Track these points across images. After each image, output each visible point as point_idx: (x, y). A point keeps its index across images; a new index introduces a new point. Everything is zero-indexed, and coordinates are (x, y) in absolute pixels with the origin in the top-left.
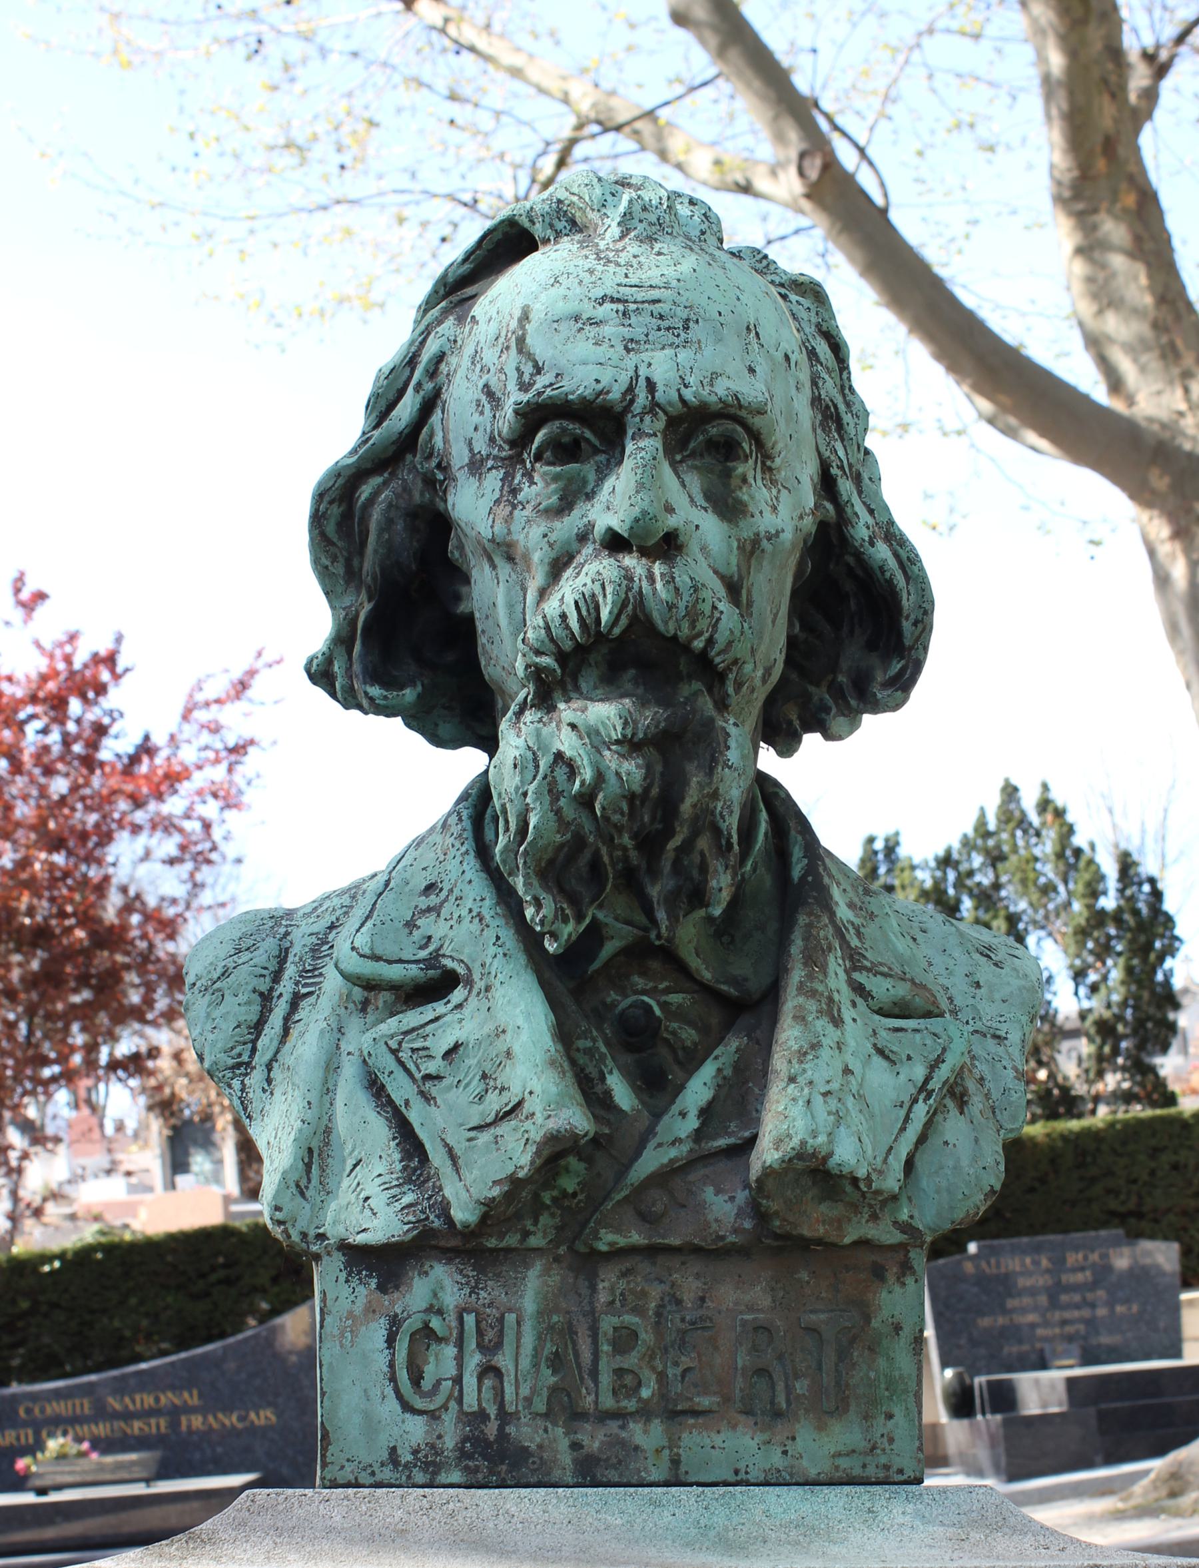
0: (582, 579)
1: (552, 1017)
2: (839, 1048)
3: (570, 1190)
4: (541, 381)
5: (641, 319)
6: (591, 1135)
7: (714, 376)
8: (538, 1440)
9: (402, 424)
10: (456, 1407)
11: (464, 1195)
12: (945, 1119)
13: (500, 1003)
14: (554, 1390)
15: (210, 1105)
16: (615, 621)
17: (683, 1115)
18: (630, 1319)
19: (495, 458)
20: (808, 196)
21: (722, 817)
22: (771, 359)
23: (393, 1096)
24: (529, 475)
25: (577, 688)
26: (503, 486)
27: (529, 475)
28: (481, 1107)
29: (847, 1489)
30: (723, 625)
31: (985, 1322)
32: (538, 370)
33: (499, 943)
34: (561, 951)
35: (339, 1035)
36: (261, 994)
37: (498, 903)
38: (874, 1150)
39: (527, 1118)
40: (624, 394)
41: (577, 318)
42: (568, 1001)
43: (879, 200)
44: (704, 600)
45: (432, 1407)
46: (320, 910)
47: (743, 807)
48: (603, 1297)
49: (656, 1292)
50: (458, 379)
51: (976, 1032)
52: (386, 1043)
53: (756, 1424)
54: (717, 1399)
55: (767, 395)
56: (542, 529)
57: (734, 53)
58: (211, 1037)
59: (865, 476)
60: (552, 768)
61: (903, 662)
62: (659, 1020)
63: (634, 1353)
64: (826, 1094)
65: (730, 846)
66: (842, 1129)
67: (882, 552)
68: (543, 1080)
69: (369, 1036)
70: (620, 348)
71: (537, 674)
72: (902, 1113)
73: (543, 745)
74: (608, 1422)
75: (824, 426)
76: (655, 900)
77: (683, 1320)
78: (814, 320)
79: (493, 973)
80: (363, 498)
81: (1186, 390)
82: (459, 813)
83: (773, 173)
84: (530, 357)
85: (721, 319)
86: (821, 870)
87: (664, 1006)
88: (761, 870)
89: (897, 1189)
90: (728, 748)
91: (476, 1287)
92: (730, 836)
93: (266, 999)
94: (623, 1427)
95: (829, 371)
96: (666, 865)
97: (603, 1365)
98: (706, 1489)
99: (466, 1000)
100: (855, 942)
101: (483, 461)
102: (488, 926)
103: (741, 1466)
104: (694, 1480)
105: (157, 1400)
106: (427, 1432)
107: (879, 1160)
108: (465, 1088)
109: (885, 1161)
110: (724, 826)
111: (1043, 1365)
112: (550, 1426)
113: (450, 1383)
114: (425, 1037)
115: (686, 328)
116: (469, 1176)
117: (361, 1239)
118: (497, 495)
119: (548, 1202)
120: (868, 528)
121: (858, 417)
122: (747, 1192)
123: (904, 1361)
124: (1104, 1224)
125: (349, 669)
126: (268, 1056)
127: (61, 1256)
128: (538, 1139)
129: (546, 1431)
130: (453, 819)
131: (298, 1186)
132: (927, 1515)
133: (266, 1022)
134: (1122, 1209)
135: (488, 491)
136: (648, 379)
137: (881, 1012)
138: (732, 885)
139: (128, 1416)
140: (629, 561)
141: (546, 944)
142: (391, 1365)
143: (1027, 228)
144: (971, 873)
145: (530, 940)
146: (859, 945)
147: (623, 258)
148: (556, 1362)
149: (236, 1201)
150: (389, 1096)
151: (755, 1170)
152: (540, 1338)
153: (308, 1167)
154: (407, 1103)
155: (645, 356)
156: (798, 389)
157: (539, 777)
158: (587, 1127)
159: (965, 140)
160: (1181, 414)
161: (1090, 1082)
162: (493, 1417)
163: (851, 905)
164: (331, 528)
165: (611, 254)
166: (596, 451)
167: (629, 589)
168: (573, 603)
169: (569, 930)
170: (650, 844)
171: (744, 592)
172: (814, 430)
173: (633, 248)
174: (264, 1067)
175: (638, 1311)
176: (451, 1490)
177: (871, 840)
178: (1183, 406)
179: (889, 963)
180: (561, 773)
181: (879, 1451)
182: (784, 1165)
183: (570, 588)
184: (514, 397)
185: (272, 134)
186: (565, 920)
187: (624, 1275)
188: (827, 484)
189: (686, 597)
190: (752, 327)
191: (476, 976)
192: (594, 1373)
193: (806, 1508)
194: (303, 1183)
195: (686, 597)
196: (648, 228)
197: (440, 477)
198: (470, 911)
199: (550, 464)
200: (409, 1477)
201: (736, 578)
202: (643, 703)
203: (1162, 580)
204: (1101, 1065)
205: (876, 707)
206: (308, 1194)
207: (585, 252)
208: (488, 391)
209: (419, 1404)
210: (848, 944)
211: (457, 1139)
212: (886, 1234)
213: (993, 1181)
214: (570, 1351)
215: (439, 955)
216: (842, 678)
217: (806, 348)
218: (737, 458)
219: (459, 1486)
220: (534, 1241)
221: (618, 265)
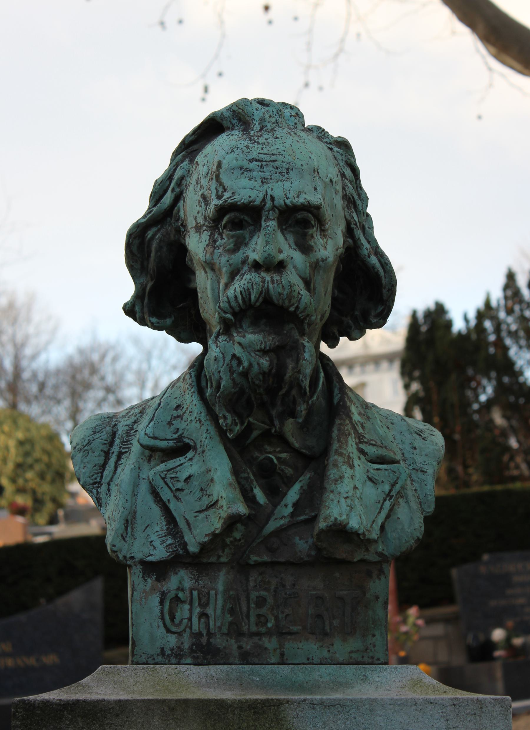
0: (243, 282)
1: (230, 464)
2: (352, 478)
3: (238, 538)
5: (268, 169)
6: (247, 515)
7: (299, 193)
8: (224, 645)
9: (166, 206)
10: (189, 631)
11: (193, 540)
12: (398, 508)
13: (208, 458)
14: (231, 624)
17: (286, 506)
18: (263, 593)
19: (207, 226)
21: (302, 381)
22: (325, 183)
23: (163, 498)
24: (221, 234)
25: (241, 327)
26: (210, 239)
27: (221, 234)
28: (200, 503)
29: (355, 666)
30: (302, 301)
31: (493, 603)
32: (225, 190)
33: (208, 432)
34: (234, 437)
35: (139, 471)
36: (105, 452)
37: (207, 415)
38: (366, 521)
39: (220, 508)
40: (261, 202)
41: (241, 168)
44: (294, 291)
45: (179, 631)
46: (129, 414)
47: (311, 378)
48: (252, 584)
50: (190, 188)
51: (414, 469)
52: (160, 475)
53: (317, 638)
54: (300, 628)
55: (322, 199)
56: (227, 258)
58: (83, 471)
59: (366, 226)
60: (231, 361)
61: (383, 307)
62: (276, 465)
63: (265, 608)
64: (346, 498)
65: (305, 393)
66: (353, 513)
67: (374, 260)
68: (226, 492)
69: (152, 472)
70: (259, 182)
72: (379, 506)
74: (254, 637)
75: (348, 207)
76: (274, 416)
77: (286, 594)
78: (344, 159)
79: (206, 445)
80: (149, 236)
82: (190, 374)
84: (221, 184)
85: (303, 168)
86: (346, 399)
87: (278, 459)
88: (321, 399)
89: (376, 538)
90: (305, 352)
91: (198, 579)
92: (305, 389)
93: (107, 454)
94: (260, 640)
95: (351, 182)
97: (252, 613)
98: (296, 666)
99: (194, 456)
100: (361, 430)
101: (201, 227)
102: (203, 425)
103: (310, 656)
104: (290, 662)
106: (177, 641)
107: (369, 526)
108: (193, 494)
109: (371, 526)
110: (303, 385)
112: (229, 639)
113: (187, 620)
114: (177, 472)
115: (288, 172)
116: (196, 532)
117: (150, 559)
118: (207, 242)
119: (229, 543)
120: (367, 250)
121: (363, 200)
122: (313, 539)
123: (380, 612)
125: (142, 309)
126: (108, 479)
128: (224, 517)
129: (227, 641)
130: (187, 377)
131: (122, 536)
132: (388, 677)
133: (107, 464)
135: (204, 240)
136: (271, 196)
137: (372, 462)
138: (306, 409)
141: (228, 434)
142: (162, 613)
145: (222, 433)
146: (363, 432)
147: (262, 140)
148: (232, 612)
150: (160, 497)
151: (316, 531)
152: (225, 601)
153: (126, 528)
154: (169, 500)
155: (270, 185)
156: (336, 194)
157: (225, 365)
158: (245, 512)
162: (205, 635)
163: (360, 414)
164: (135, 249)
165: (256, 138)
166: (250, 225)
167: (263, 286)
168: (239, 292)
169: (238, 429)
171: (312, 285)
172: (343, 209)
174: (106, 484)
176: (187, 666)
179: (375, 439)
180: (234, 363)
181: (369, 651)
182: (328, 528)
183: (238, 285)
184: (215, 202)
186: (236, 425)
187: (261, 574)
188: (349, 232)
189: (287, 290)
190: (316, 170)
191: (198, 447)
192: (248, 616)
194: (124, 535)
195: (287, 290)
196: (272, 125)
197: (182, 229)
198: (196, 418)
199: (230, 231)
200: (169, 661)
201: (308, 279)
205: (373, 326)
206: (126, 539)
207: (245, 137)
208: (204, 197)
209: (173, 629)
210: (357, 431)
211: (190, 517)
212: (372, 557)
213: (419, 535)
214: (238, 607)
215: (182, 437)
216: (357, 313)
217: (340, 172)
218: (309, 228)
219: (190, 664)
220: (223, 560)
221: (258, 143)
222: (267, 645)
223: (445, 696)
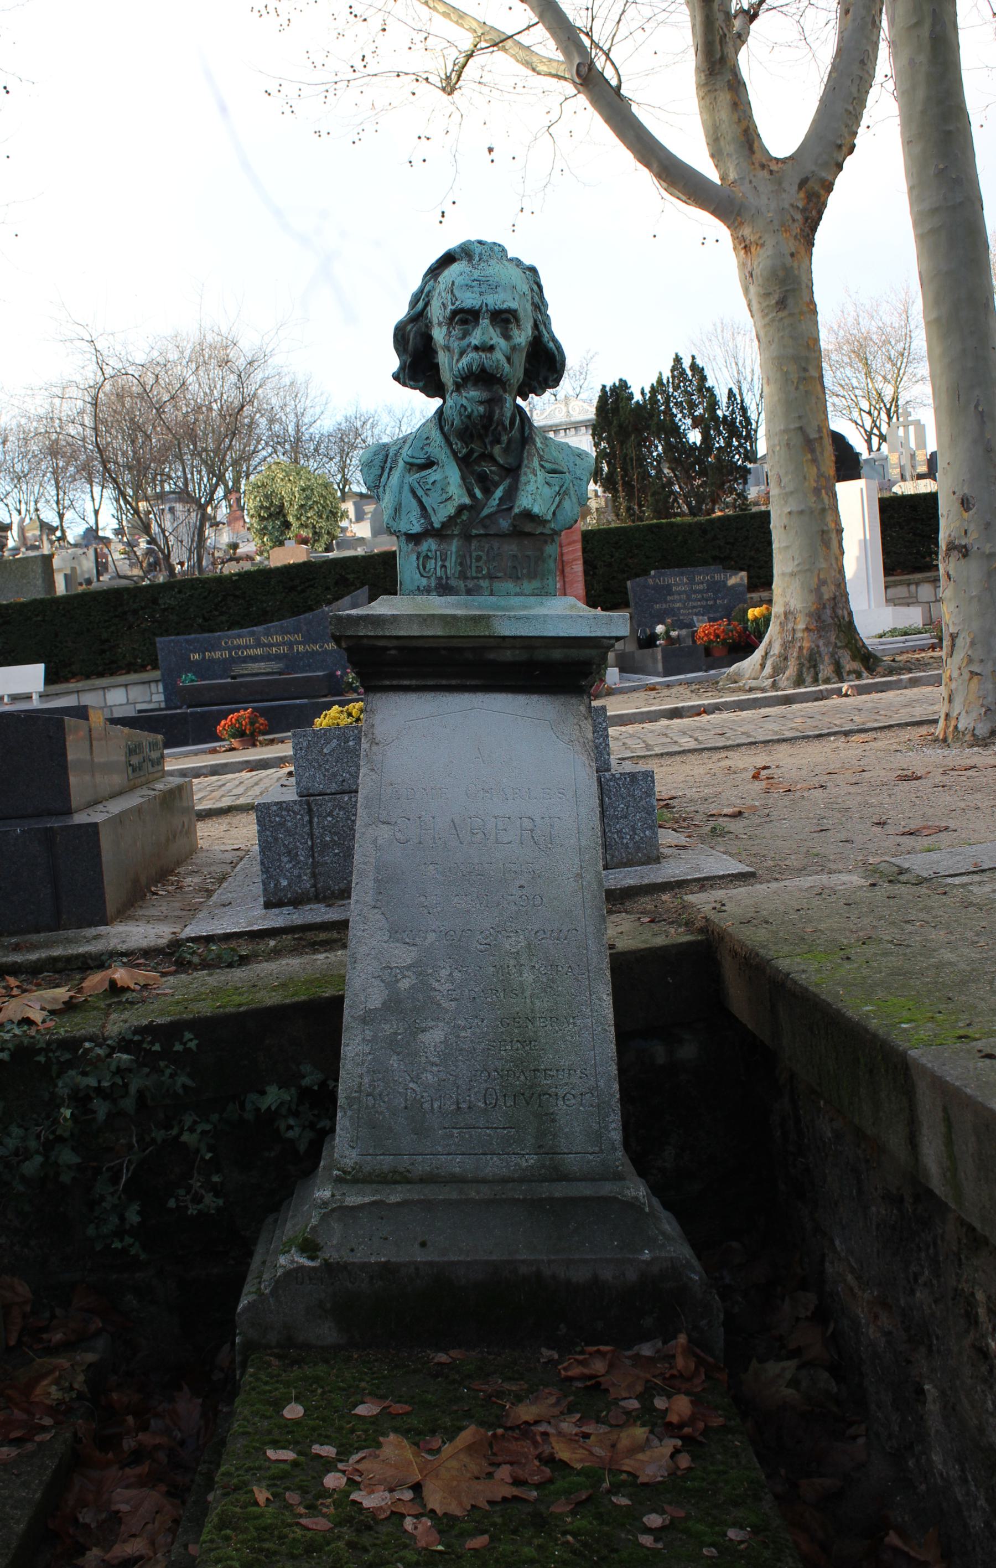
14: (460, 572)
24: (454, 328)
27: (454, 328)
31: (658, 606)
42: (464, 469)
43: (614, 82)
48: (473, 547)
49: (487, 546)
50: (435, 298)
67: (551, 345)
93: (383, 469)
105: (283, 638)
137: (548, 472)
139: (270, 645)
145: (455, 454)
147: (480, 267)
148: (461, 564)
152: (457, 558)
164: (399, 337)
169: (464, 451)
170: (486, 428)
175: (483, 551)
180: (462, 410)
183: (465, 361)
184: (450, 307)
188: (536, 326)
212: (547, 531)
220: (455, 532)
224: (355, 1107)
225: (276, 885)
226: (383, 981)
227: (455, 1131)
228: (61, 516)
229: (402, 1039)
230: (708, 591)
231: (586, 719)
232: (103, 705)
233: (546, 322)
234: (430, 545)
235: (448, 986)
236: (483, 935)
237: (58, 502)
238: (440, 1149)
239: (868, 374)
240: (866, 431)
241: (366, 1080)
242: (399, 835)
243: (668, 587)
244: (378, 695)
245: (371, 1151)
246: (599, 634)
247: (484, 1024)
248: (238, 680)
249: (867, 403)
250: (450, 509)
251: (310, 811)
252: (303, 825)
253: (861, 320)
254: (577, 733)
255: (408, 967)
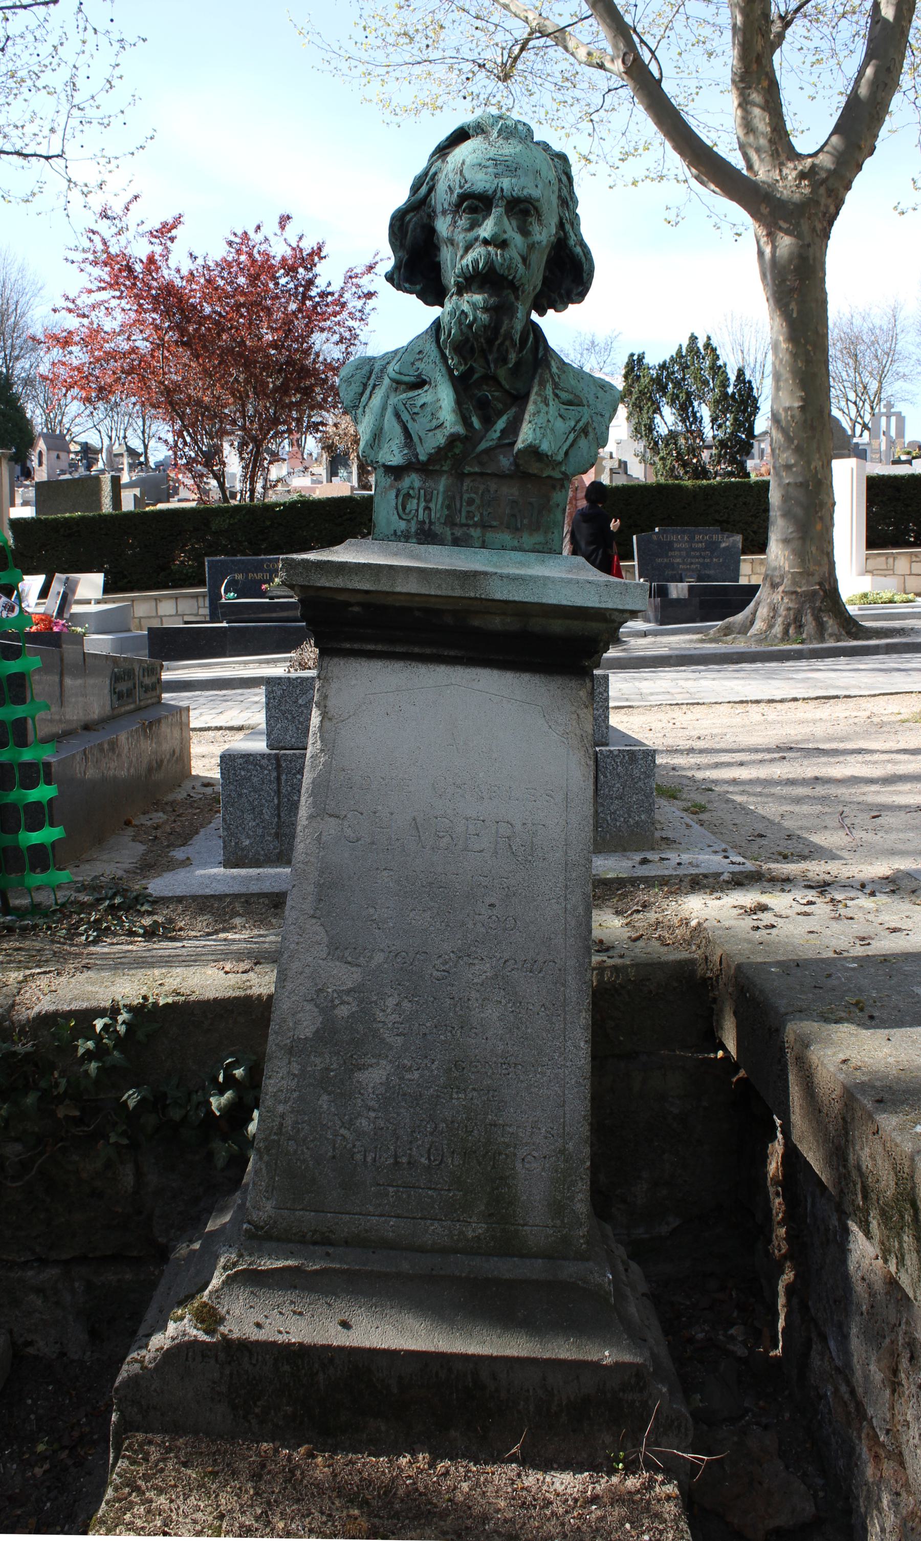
4: (467, 186)
7: (524, 188)
14: (447, 516)
15: (348, 448)
16: (484, 268)
17: (495, 431)
18: (473, 495)
20: (625, 73)
31: (659, 560)
32: (466, 182)
41: (480, 165)
43: (657, 75)
48: (465, 488)
49: (482, 487)
57: (600, 5)
60: (460, 315)
67: (578, 249)
71: (457, 284)
73: (458, 308)
75: (562, 206)
81: (781, 171)
83: (612, 61)
84: (464, 177)
87: (492, 396)
96: (495, 349)
100: (557, 380)
111: (681, 581)
123: (559, 516)
124: (713, 525)
127: (284, 504)
134: (721, 519)
137: (563, 403)
140: (490, 248)
143: (722, 92)
144: (673, 373)
145: (450, 371)
148: (449, 507)
149: (356, 489)
152: (444, 499)
153: (374, 440)
159: (699, 50)
160: (777, 181)
161: (714, 466)
163: (558, 368)
164: (396, 229)
166: (483, 211)
169: (462, 368)
170: (490, 342)
173: (501, 142)
175: (476, 493)
177: (632, 355)
178: (778, 178)
180: (463, 317)
184: (458, 191)
185: (398, 28)
187: (472, 481)
188: (561, 225)
192: (460, 511)
193: (523, 558)
202: (490, 296)
203: (761, 253)
204: (718, 459)
205: (573, 303)
209: (404, 517)
216: (563, 291)
220: (445, 468)
222: (473, 533)
223: (600, 579)
224: (273, 1151)
225: (236, 843)
226: (317, 1006)
227: (391, 1189)
228: (146, 447)
229: (335, 1076)
230: (705, 549)
231: (587, 707)
232: (154, 614)
233: (575, 221)
234: (413, 480)
235: (394, 1017)
236: (441, 960)
237: (143, 432)
238: (371, 1209)
239: (856, 370)
240: (851, 419)
241: (289, 1121)
242: (349, 832)
243: (670, 543)
244: (336, 660)
245: (288, 1205)
246: (610, 605)
247: (434, 1067)
248: (276, 600)
249: (854, 394)
250: (440, 439)
251: (279, 766)
252: (270, 781)
253: (854, 321)
254: (574, 723)
255: (349, 992)
